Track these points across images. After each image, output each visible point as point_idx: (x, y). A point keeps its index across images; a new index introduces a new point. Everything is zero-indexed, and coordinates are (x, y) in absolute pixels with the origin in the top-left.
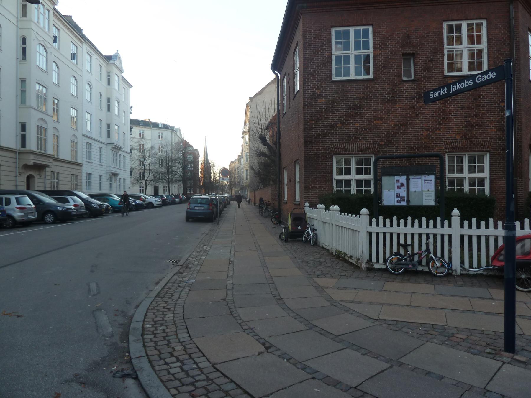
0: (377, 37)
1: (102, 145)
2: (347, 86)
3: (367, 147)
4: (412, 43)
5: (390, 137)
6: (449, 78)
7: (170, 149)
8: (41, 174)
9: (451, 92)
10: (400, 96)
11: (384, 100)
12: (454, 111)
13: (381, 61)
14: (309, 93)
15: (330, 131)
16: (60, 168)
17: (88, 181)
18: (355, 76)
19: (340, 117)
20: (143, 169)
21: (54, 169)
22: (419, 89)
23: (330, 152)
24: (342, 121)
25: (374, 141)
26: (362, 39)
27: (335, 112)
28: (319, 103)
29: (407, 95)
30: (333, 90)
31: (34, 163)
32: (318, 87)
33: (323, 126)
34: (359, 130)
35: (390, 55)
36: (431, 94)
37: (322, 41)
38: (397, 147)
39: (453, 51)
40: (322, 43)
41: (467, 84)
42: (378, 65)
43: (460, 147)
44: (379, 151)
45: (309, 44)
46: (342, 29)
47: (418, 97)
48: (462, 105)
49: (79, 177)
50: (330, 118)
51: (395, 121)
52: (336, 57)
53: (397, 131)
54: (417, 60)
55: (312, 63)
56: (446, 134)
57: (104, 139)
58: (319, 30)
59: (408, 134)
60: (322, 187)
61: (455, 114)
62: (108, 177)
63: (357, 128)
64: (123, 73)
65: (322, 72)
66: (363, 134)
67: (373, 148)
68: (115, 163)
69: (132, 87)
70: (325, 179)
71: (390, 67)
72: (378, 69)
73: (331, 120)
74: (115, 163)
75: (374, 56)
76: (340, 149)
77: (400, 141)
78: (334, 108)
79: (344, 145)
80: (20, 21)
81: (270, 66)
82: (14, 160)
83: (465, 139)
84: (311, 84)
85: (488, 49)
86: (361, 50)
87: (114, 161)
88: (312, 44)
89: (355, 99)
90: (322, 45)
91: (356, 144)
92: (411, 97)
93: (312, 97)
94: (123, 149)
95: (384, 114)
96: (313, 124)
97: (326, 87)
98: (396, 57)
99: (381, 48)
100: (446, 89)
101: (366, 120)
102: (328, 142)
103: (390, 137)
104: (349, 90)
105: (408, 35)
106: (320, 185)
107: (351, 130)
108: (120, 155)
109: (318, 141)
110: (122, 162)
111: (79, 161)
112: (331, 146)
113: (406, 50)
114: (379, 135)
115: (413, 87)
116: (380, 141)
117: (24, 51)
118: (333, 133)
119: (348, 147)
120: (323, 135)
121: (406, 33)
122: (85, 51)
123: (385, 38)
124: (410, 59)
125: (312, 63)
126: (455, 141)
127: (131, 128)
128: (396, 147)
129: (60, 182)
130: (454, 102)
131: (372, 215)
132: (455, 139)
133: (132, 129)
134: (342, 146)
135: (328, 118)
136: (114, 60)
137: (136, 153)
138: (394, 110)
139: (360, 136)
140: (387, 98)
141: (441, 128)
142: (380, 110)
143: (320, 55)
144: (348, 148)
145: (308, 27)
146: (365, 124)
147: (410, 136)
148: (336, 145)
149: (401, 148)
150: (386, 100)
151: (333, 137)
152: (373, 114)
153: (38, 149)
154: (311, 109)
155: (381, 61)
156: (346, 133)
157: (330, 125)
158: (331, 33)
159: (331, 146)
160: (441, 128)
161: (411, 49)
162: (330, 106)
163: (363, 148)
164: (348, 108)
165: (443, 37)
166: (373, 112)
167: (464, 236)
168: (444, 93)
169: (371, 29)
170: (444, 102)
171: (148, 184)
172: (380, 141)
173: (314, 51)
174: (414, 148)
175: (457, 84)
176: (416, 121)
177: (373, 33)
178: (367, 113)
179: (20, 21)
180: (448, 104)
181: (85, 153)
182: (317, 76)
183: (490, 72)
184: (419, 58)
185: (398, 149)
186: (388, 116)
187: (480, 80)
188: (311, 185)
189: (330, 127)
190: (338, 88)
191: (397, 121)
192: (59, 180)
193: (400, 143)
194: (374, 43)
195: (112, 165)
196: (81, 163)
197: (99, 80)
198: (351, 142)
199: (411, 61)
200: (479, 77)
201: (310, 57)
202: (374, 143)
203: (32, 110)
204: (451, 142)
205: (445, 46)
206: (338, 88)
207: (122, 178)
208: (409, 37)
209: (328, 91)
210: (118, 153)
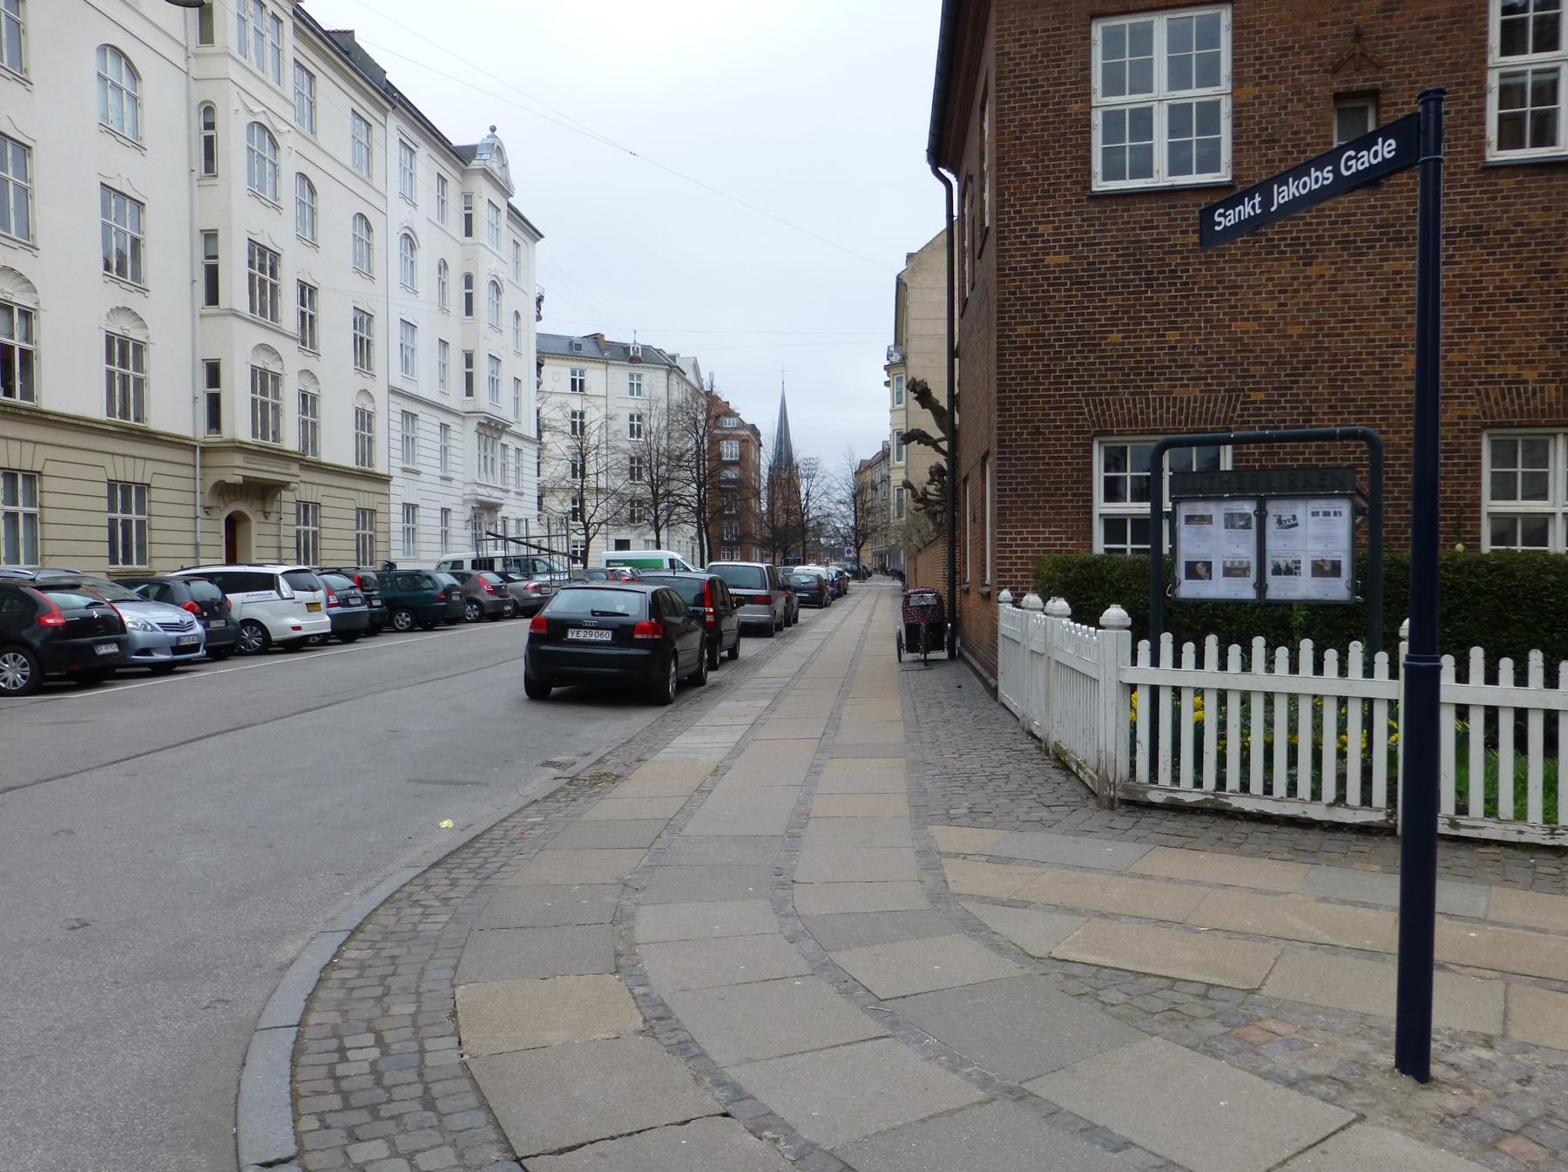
0: (1246, 40)
1: (447, 419)
2: (1141, 209)
3: (1208, 408)
4: (1369, 55)
5: (1287, 375)
6: (1501, 173)
7: (664, 424)
8: (268, 510)
9: (1273, 209)
10: (1323, 237)
11: (1267, 253)
12: (1519, 284)
13: (1260, 123)
14: (1016, 237)
15: (1084, 358)
16: (323, 490)
17: (408, 529)
18: (1171, 173)
19: (1117, 312)
20: (577, 487)
21: (307, 493)
22: (1393, 212)
23: (1083, 426)
24: (1123, 324)
25: (1233, 390)
26: (1194, 52)
27: (1100, 295)
28: (1048, 266)
29: (1348, 235)
30: (1094, 225)
31: (244, 476)
32: (1043, 216)
33: (1060, 340)
34: (1181, 354)
35: (1292, 100)
36: (1220, 215)
37: (1059, 66)
38: (1310, 408)
39: (1524, 73)
40: (1059, 72)
41: (1317, 179)
42: (1248, 137)
43: (1535, 409)
44: (1249, 422)
45: (1015, 77)
46: (1127, 21)
47: (1388, 240)
48: (1547, 264)
49: (379, 517)
50: (1083, 314)
51: (1304, 323)
52: (1105, 114)
53: (1310, 356)
54: (1386, 112)
55: (1027, 138)
56: (1487, 363)
57: (456, 400)
58: (1048, 30)
59: (1348, 367)
60: (1056, 539)
61: (1521, 293)
62: (468, 513)
63: (1175, 348)
64: (512, 196)
65: (1059, 165)
66: (1192, 366)
67: (1227, 413)
68: (489, 471)
69: (542, 236)
70: (1066, 514)
71: (1289, 140)
72: (1248, 150)
73: (1087, 320)
74: (489, 471)
75: (1234, 106)
76: (1117, 415)
77: (1320, 390)
78: (1099, 282)
79: (1128, 402)
80: (196, 56)
81: (925, 154)
82: (188, 471)
83: (1553, 381)
84: (1021, 205)
85: (1485, 61)
86: (1189, 87)
87: (486, 464)
88: (1027, 75)
89: (1168, 253)
90: (1059, 78)
91: (1168, 399)
92: (1362, 241)
93: (1024, 249)
94: (514, 428)
95: (1267, 299)
96: (1027, 335)
97: (1070, 214)
98: (1310, 105)
99: (1260, 78)
100: (1258, 199)
101: (1206, 321)
102: (1077, 395)
103: (1287, 375)
104: (1147, 222)
105: (1357, 28)
106: (1051, 533)
107: (1154, 355)
108: (504, 446)
109: (1044, 390)
110: (512, 467)
111: (380, 468)
112: (1088, 405)
113: (1348, 82)
114: (1248, 370)
115: (1369, 207)
116: (1250, 390)
117: (209, 144)
118: (1094, 364)
119: (1141, 409)
120: (1061, 371)
121: (1352, 21)
122: (394, 137)
123: (1274, 43)
124: (1365, 109)
125: (1027, 138)
126: (1518, 390)
127: (540, 365)
128: (1306, 408)
129: (325, 533)
130: (1519, 252)
131: (1141, 629)
132: (1518, 380)
133: (542, 365)
134: (1122, 408)
135: (1078, 315)
136: (484, 157)
137: (560, 445)
138: (1301, 284)
139: (1183, 373)
140: (1279, 246)
141: (1467, 343)
142: (1254, 286)
143: (1053, 110)
144: (1142, 413)
145: (1013, 22)
146: (1200, 334)
147: (1354, 373)
148: (1101, 404)
149: (1325, 414)
150: (1272, 253)
151: (1094, 376)
152: (1229, 300)
153: (254, 434)
154: (1020, 287)
155: (1260, 123)
156: (1135, 362)
157: (1084, 339)
158: (1089, 38)
159: (1088, 405)
160: (1467, 343)
161: (1368, 76)
162: (1083, 277)
163: (1194, 413)
164: (1143, 283)
165: (1486, 26)
166: (1227, 292)
167: (1471, 708)
168: (1252, 214)
169: (1225, 15)
170: (1482, 255)
171: (594, 534)
172: (1250, 390)
173: (1031, 99)
174: (1368, 413)
175: (1291, 179)
176: (1379, 320)
177: (1234, 28)
178: (1206, 296)
179: (196, 56)
180: (1495, 261)
181: (399, 445)
182: (1043, 179)
183: (1380, 140)
184: (1396, 104)
185: (1312, 414)
186: (1281, 305)
187: (1351, 166)
188: (1022, 533)
189: (1083, 345)
190: (1110, 218)
191: (1312, 323)
192: (376, 532)
193: (1322, 394)
194: (1237, 62)
195: (479, 477)
196: (387, 473)
197: (439, 223)
198: (1153, 393)
199: (1367, 113)
200: (1349, 158)
201: (1021, 119)
202: (1230, 397)
203: (235, 322)
204: (1502, 390)
205: (1495, 57)
206: (1110, 218)
207: (511, 516)
208: (1358, 36)
209: (1077, 226)
210: (499, 442)
